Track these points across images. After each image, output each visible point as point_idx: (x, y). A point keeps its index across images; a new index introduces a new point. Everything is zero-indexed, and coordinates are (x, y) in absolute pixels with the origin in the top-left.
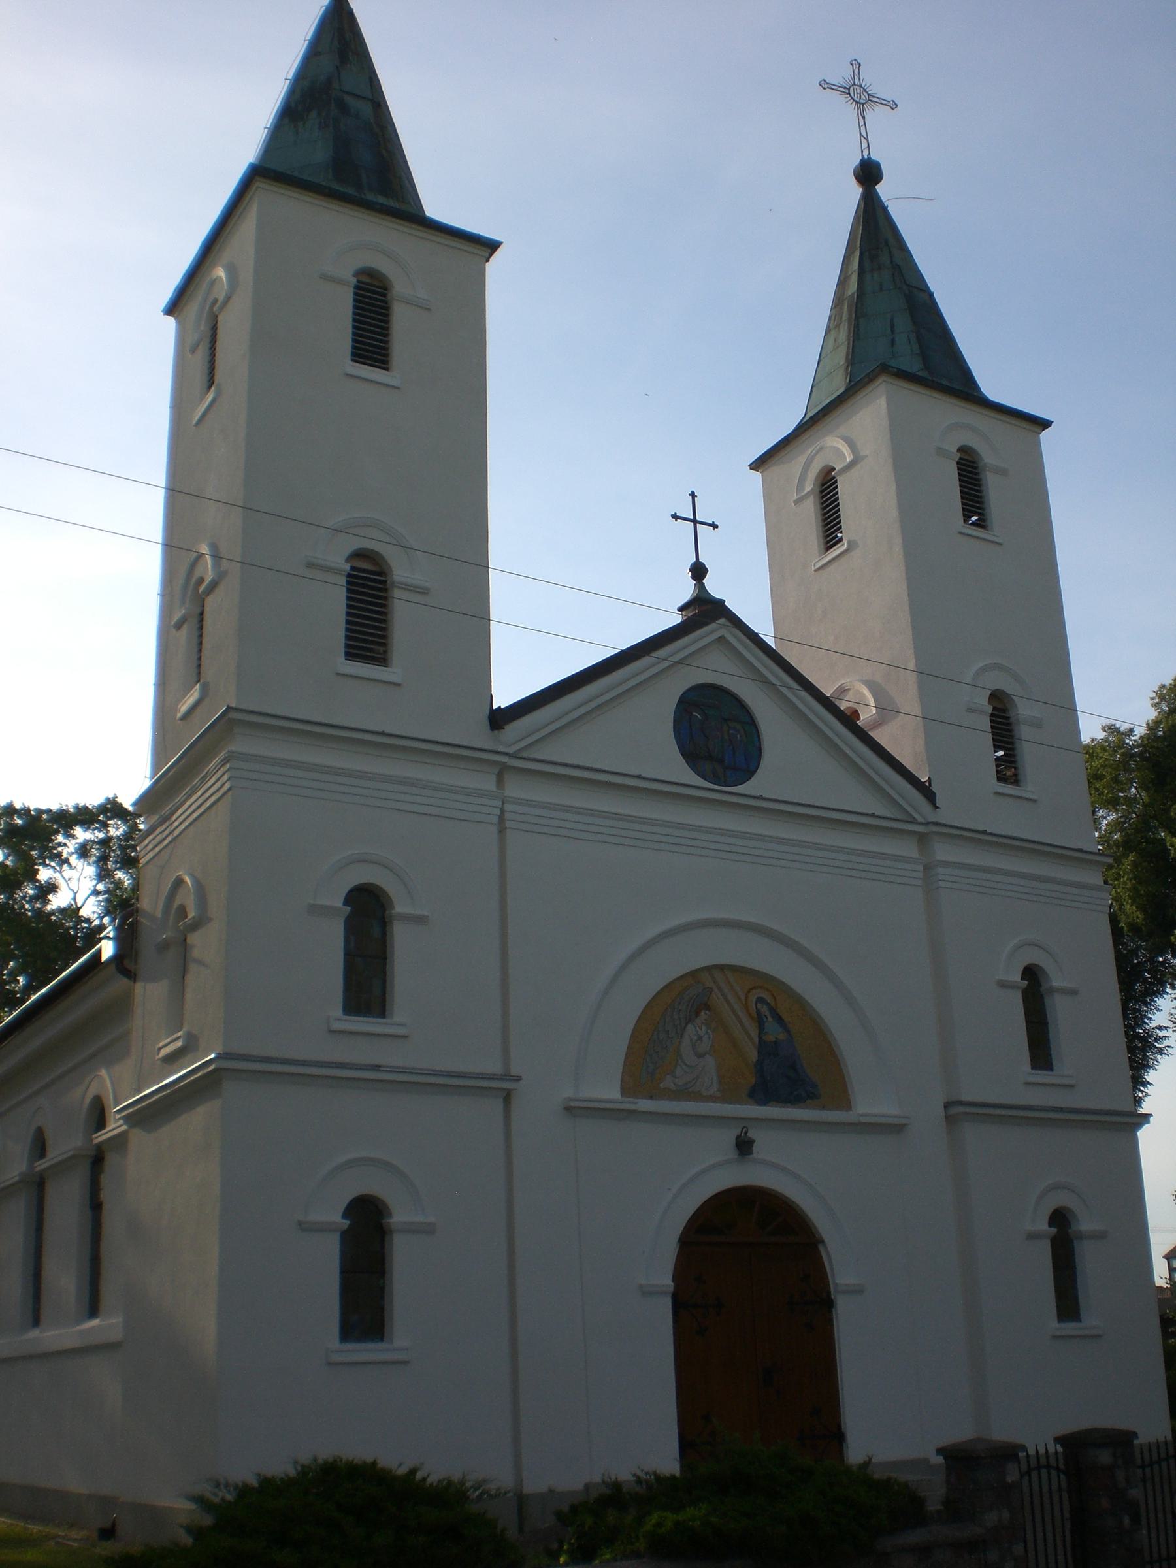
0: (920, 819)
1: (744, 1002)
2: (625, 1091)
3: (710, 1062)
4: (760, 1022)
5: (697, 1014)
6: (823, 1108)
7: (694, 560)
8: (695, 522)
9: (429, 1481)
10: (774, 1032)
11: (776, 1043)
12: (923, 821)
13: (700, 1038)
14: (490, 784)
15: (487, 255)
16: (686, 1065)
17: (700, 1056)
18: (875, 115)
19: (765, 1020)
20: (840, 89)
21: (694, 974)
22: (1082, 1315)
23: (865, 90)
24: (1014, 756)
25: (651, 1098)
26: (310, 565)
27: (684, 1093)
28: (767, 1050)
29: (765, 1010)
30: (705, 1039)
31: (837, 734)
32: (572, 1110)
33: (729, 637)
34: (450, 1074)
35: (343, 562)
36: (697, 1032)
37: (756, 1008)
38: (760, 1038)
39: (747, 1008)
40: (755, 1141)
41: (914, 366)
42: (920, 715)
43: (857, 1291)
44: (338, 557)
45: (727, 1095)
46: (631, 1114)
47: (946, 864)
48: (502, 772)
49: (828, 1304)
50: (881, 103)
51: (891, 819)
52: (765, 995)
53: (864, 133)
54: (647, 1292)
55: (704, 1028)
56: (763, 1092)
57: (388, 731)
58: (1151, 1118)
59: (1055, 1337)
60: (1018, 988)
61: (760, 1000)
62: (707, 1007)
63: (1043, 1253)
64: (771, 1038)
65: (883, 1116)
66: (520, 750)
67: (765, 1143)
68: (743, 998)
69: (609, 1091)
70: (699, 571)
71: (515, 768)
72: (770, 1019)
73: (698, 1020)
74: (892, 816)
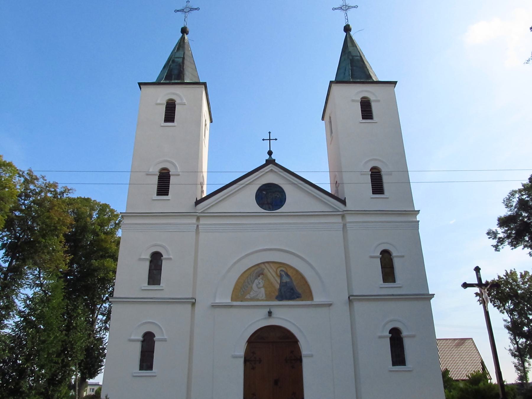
0: (341, 210)
2: (232, 301)
3: (263, 290)
4: (281, 276)
5: (259, 276)
6: (302, 300)
7: (269, 150)
8: (270, 140)
10: (285, 279)
12: (342, 211)
13: (260, 283)
14: (194, 221)
15: (394, 85)
16: (254, 291)
17: (259, 288)
18: (350, 12)
20: (192, 9)
21: (258, 265)
22: (406, 364)
23: (347, 6)
25: (242, 301)
27: (252, 299)
28: (283, 285)
29: (283, 273)
30: (261, 283)
32: (214, 306)
33: (273, 169)
34: (173, 299)
37: (280, 273)
39: (276, 273)
44: (156, 170)
45: (269, 298)
46: (232, 306)
47: (350, 222)
48: (198, 218)
49: (300, 360)
50: (353, 8)
51: (331, 212)
53: (346, 18)
55: (261, 280)
56: (281, 297)
58: (435, 296)
62: (262, 274)
64: (284, 281)
66: (204, 210)
68: (275, 270)
69: (227, 300)
70: (270, 153)
71: (201, 216)
73: (259, 278)
74: (331, 211)
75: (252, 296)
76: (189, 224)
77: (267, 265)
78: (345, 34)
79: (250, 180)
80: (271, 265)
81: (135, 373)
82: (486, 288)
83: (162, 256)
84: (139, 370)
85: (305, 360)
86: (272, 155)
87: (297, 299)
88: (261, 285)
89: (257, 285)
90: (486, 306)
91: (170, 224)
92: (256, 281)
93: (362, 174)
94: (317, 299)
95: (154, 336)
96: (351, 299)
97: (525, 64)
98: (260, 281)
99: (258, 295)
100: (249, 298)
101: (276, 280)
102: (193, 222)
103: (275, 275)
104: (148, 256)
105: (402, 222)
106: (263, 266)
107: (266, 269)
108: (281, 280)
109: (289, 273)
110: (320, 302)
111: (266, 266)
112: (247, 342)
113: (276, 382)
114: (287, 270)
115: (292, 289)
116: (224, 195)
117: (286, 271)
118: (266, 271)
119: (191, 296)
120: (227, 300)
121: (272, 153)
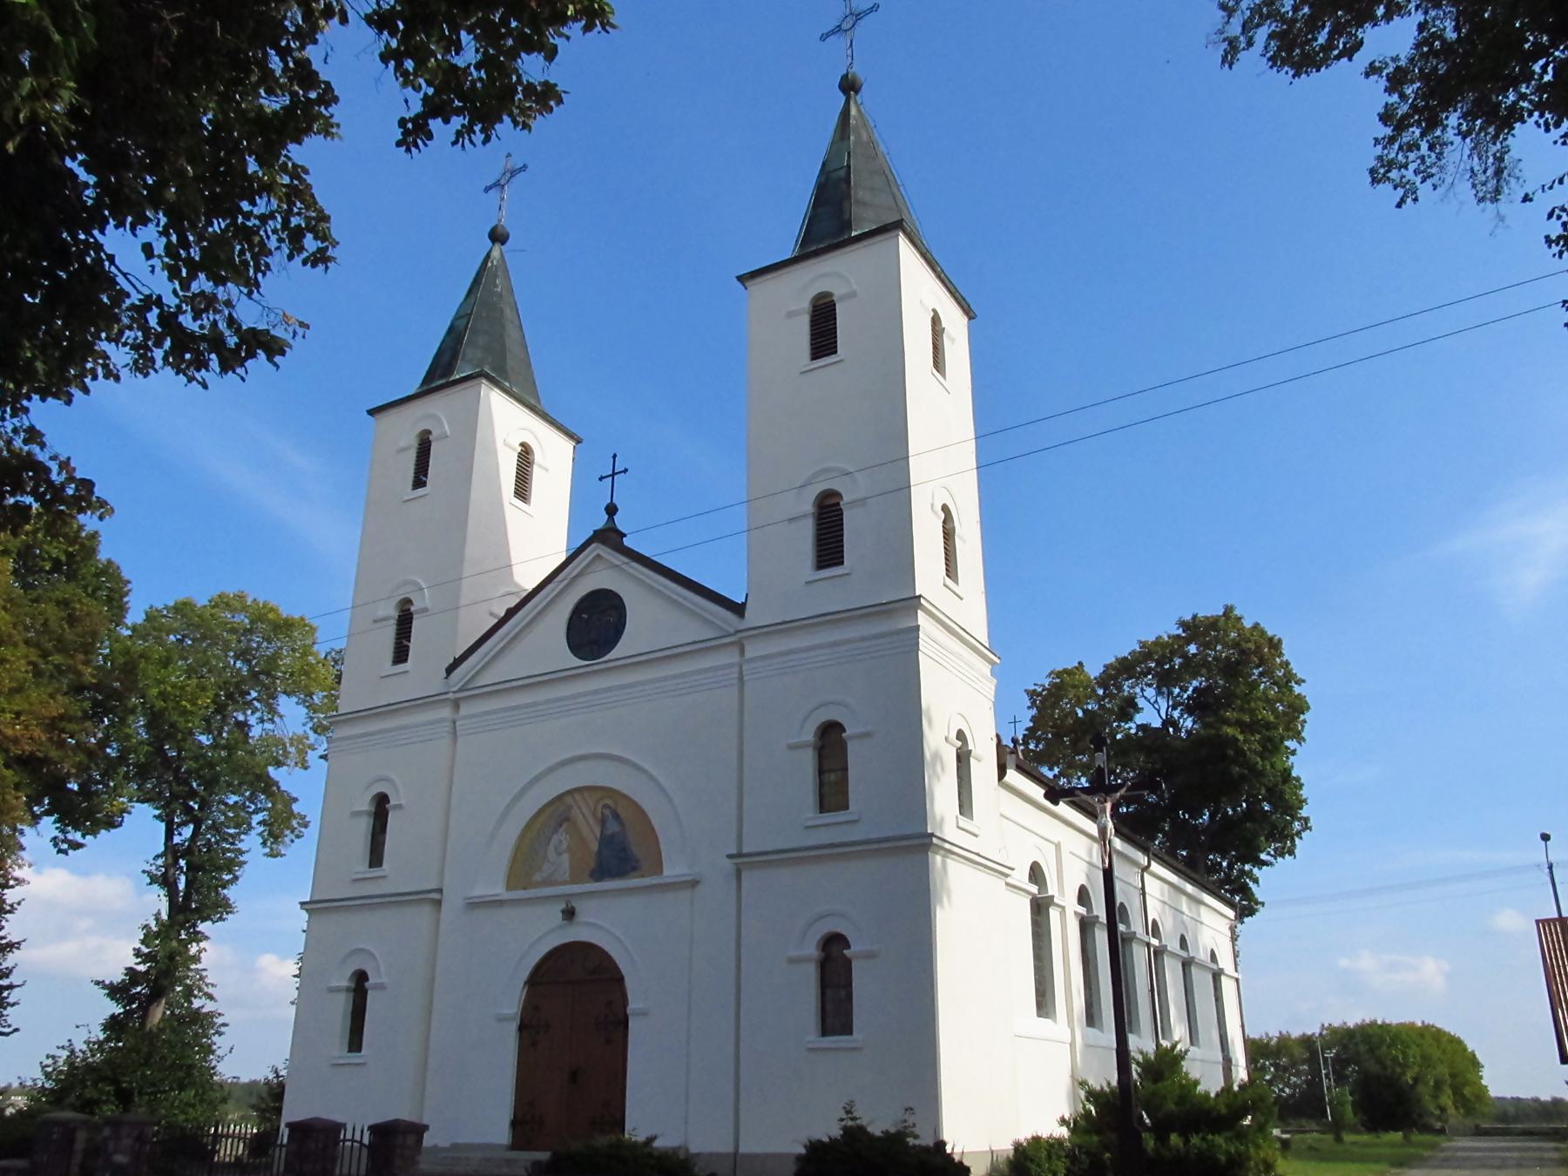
2: (509, 887)
3: (566, 858)
4: (603, 822)
5: (560, 826)
9: (657, 1144)
10: (613, 827)
21: (560, 797)
24: (397, 639)
25: (525, 889)
26: (375, 621)
27: (547, 882)
28: (606, 841)
29: (607, 812)
38: (602, 832)
39: (594, 815)
43: (644, 1014)
48: (456, 704)
52: (608, 802)
53: (849, 52)
54: (502, 1019)
56: (602, 871)
57: (697, 640)
59: (811, 1050)
60: (808, 746)
61: (606, 806)
62: (567, 819)
63: (809, 977)
64: (609, 832)
67: (585, 910)
69: (499, 890)
70: (611, 510)
73: (561, 830)
77: (577, 796)
78: (843, 98)
80: (586, 794)
81: (809, 1042)
82: (1108, 798)
84: (347, 1049)
85: (633, 1024)
86: (615, 514)
88: (564, 845)
89: (556, 848)
91: (404, 727)
94: (673, 869)
95: (367, 980)
96: (743, 861)
97: (1210, 46)
98: (562, 838)
101: (592, 830)
102: (731, 661)
103: (591, 821)
104: (809, 735)
105: (876, 637)
106: (569, 800)
107: (576, 808)
109: (621, 811)
111: (575, 801)
112: (525, 983)
113: (574, 1076)
115: (624, 849)
118: (575, 813)
119: (434, 886)
120: (499, 890)
121: (617, 510)
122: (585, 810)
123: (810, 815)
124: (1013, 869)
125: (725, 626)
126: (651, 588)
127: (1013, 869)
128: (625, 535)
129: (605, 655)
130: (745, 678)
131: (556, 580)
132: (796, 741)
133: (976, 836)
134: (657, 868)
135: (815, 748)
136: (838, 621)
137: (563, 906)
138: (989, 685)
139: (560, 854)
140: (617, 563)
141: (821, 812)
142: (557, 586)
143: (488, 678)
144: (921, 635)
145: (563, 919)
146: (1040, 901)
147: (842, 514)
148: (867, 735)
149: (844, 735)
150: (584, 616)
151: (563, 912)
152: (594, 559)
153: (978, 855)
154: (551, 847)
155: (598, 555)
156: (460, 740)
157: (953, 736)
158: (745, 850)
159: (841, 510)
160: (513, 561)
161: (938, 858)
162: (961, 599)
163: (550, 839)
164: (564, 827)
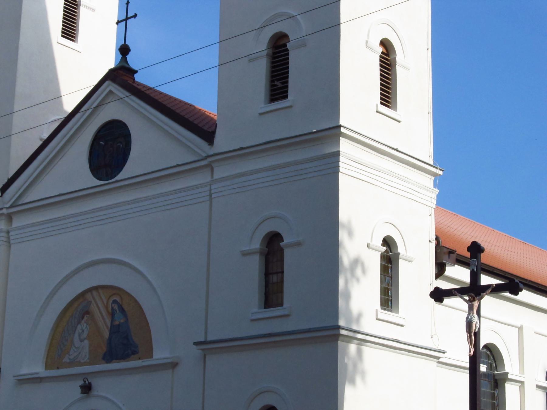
1: (106, 304)
2: (48, 367)
3: (86, 342)
4: (112, 315)
5: (83, 318)
7: (123, 43)
10: (119, 319)
11: (119, 325)
19: (115, 312)
21: (83, 294)
25: (58, 368)
27: (73, 363)
28: (115, 330)
30: (85, 331)
31: (162, 121)
35: (263, 106)
36: (82, 327)
39: (107, 307)
40: (80, 386)
41: (453, 291)
42: (125, 96)
48: (10, 218)
52: (118, 299)
55: (85, 324)
61: (115, 302)
65: (161, 359)
68: (105, 303)
69: (39, 369)
70: (124, 50)
72: (118, 312)
73: (83, 322)
74: (189, 161)
75: (72, 357)
76: (197, 187)
77: (95, 293)
79: (78, 121)
80: (101, 291)
83: (283, 241)
87: (133, 356)
88: (85, 335)
89: (79, 335)
90: (469, 339)
92: (79, 327)
93: (250, 61)
98: (83, 327)
99: (80, 353)
100: (68, 361)
103: (104, 313)
104: (257, 244)
108: (113, 320)
110: (147, 361)
114: (122, 299)
116: (40, 164)
117: (120, 303)
118: (94, 308)
120: (39, 369)
121: (129, 50)
122: (100, 305)
123: (256, 310)
124: (444, 352)
125: (199, 151)
126: (149, 119)
127: (444, 352)
128: (136, 72)
129: (115, 176)
130: (213, 196)
131: (82, 110)
132: (247, 248)
133: (402, 326)
134: (149, 353)
135: (261, 253)
136: (280, 147)
137: (81, 383)
138: (429, 194)
139: (82, 341)
140: (122, 96)
141: (265, 308)
142: (84, 114)
143: (34, 195)
144: (341, 159)
145: (82, 393)
146: (496, 378)
147: (288, 54)
148: (298, 244)
149: (281, 244)
150: (101, 143)
151: (82, 387)
152: (107, 95)
153: (398, 342)
154: (76, 335)
155: (111, 92)
156: (12, 246)
157: (378, 242)
158: (209, 338)
159: (287, 50)
160: (63, 92)
161: (353, 347)
162: (399, 122)
163: (76, 328)
164: (85, 318)
